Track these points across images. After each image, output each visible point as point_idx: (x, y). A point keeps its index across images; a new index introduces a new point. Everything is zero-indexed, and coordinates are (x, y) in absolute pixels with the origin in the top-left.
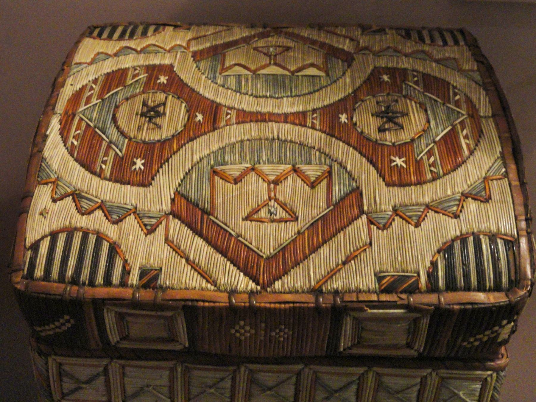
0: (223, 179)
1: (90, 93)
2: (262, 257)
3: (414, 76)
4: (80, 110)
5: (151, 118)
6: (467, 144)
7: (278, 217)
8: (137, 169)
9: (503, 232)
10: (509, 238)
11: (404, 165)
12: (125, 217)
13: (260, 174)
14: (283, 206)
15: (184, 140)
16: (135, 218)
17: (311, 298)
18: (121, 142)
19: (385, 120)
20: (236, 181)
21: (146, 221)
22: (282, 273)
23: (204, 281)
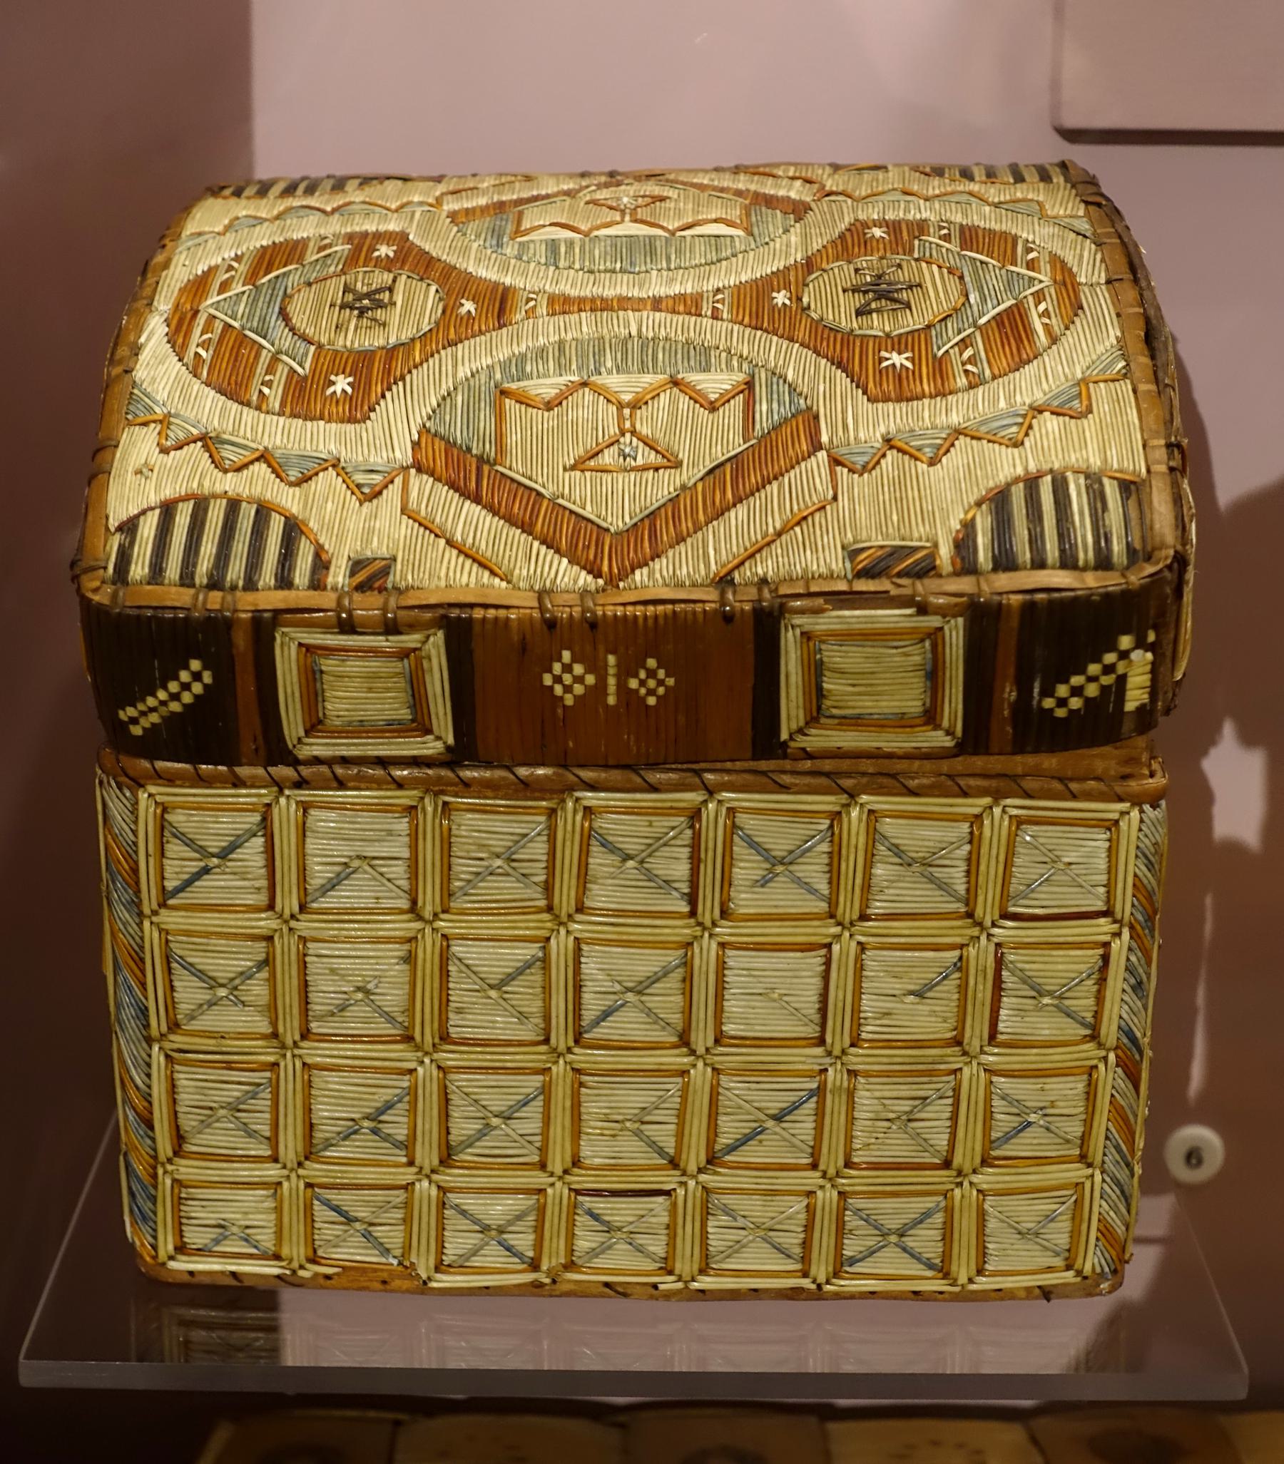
0: (521, 403)
1: (227, 276)
2: (607, 530)
3: (941, 228)
4: (209, 302)
5: (362, 312)
6: (1045, 326)
7: (640, 461)
8: (339, 392)
9: (1115, 466)
10: (1127, 477)
11: (909, 365)
12: (317, 474)
13: (598, 391)
14: (649, 444)
15: (437, 343)
16: (338, 475)
17: (712, 594)
18: (301, 351)
19: (871, 295)
20: (549, 406)
21: (360, 478)
22: (648, 556)
23: (487, 573)
